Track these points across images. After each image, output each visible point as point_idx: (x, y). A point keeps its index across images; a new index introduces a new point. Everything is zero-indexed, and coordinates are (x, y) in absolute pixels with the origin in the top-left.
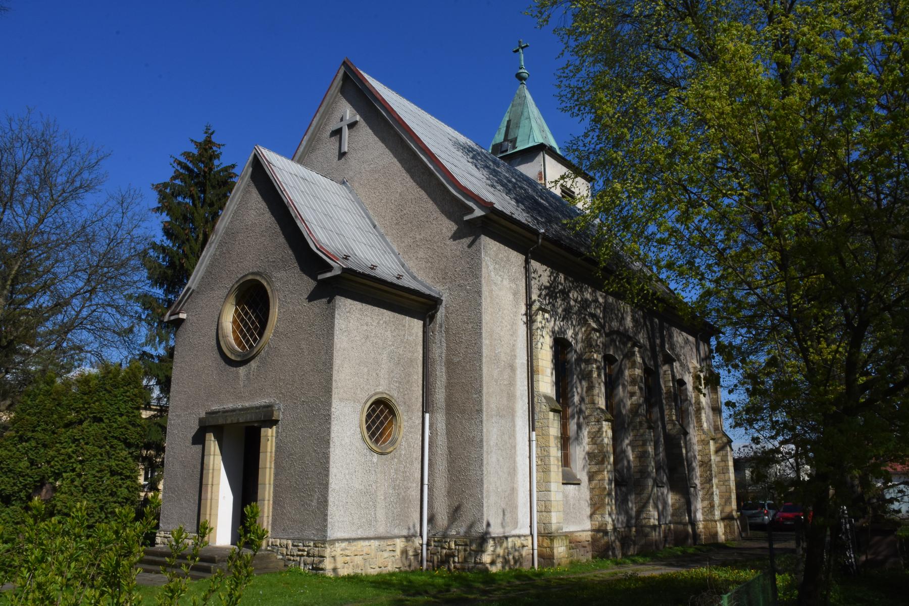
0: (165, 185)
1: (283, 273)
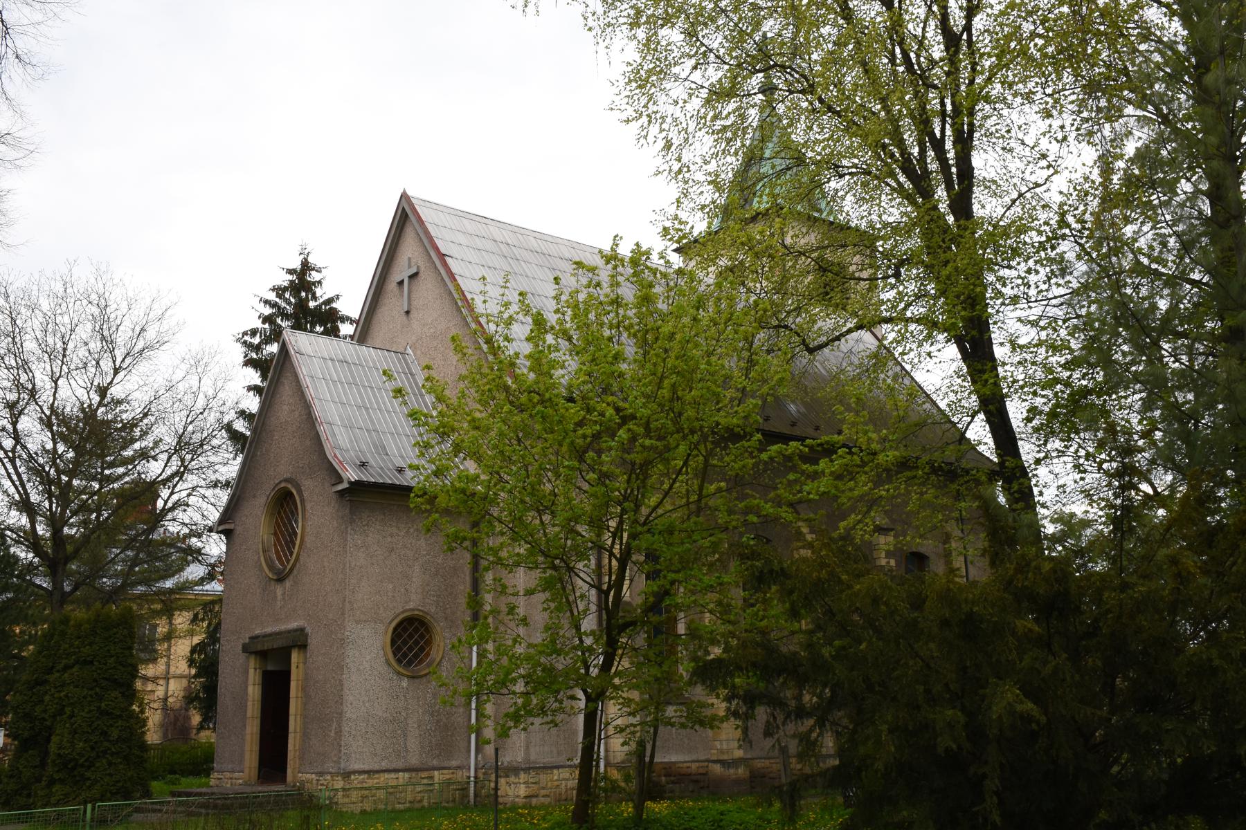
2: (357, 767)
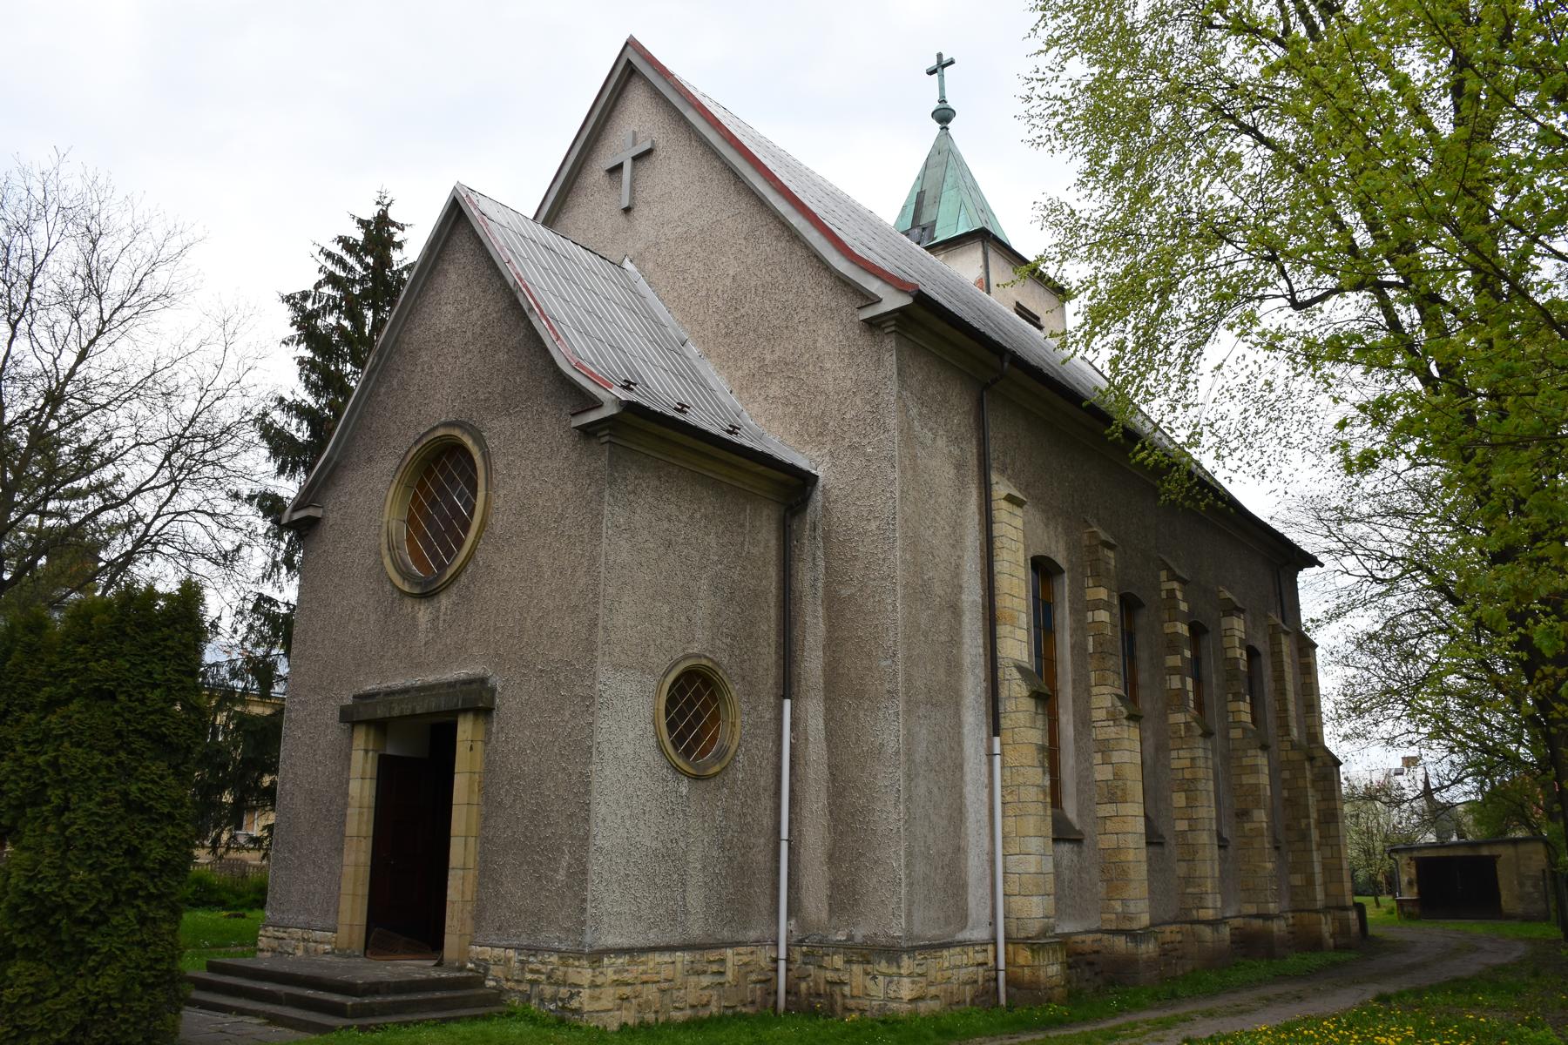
0: (305, 296)
1: (506, 422)
2: (611, 940)
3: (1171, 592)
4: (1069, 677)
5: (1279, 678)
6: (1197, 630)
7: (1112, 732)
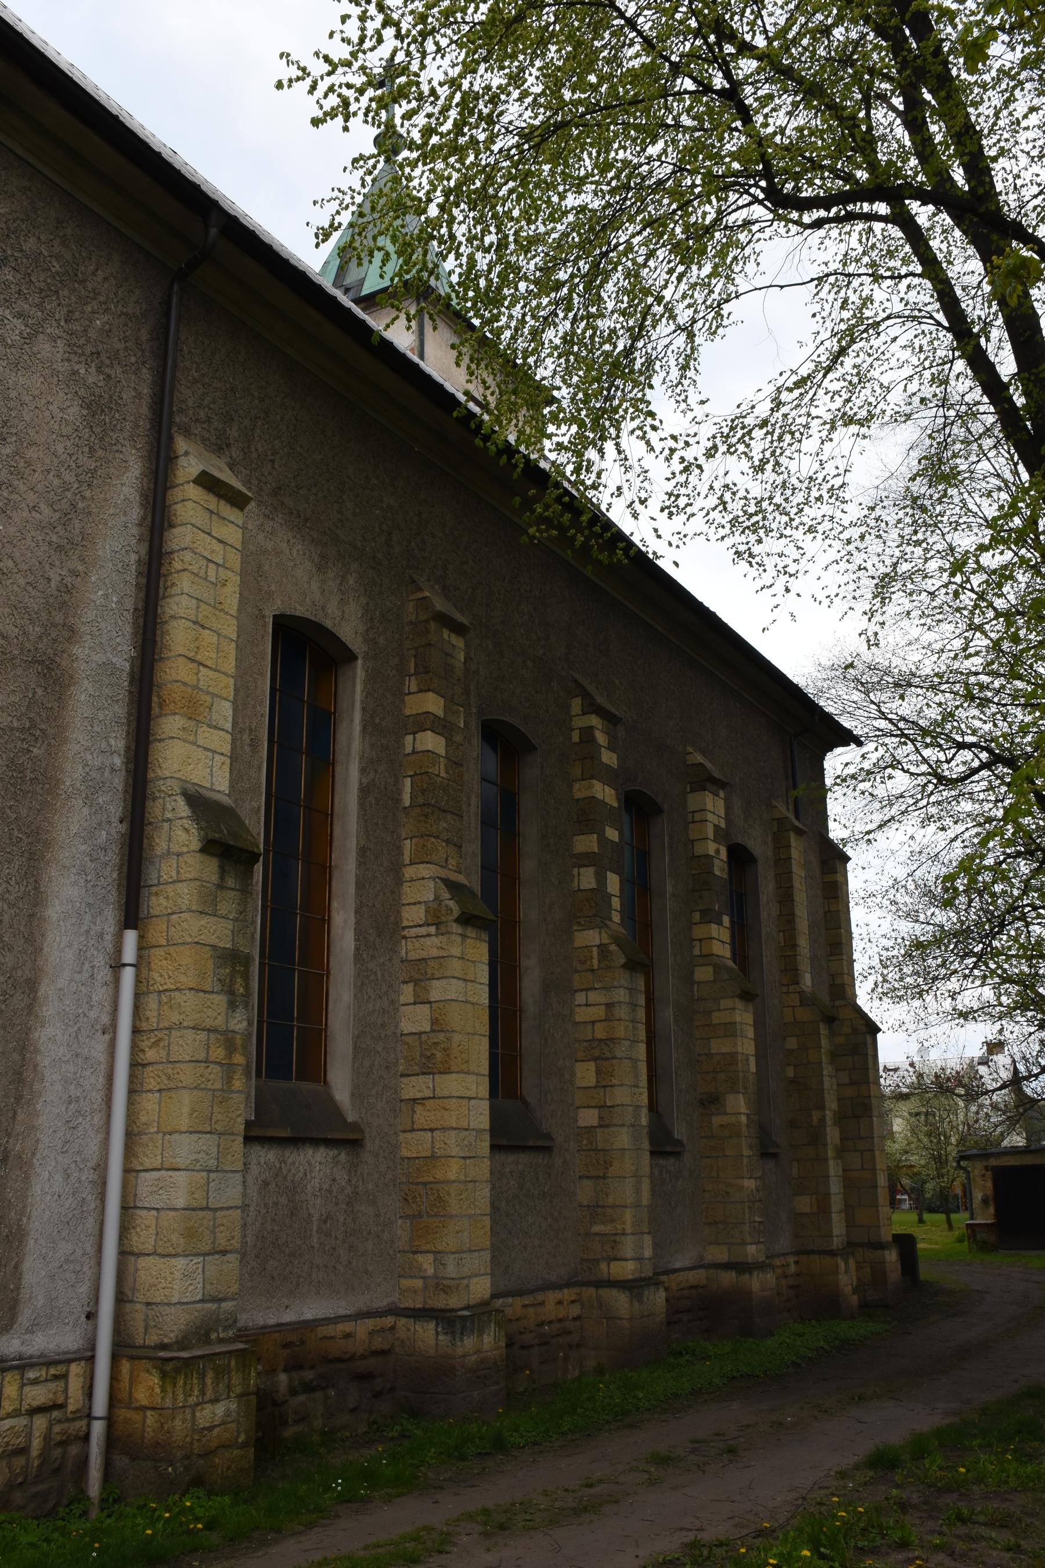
3: (587, 733)
4: (353, 844)
5: (786, 897)
6: (639, 808)
7: (432, 945)
